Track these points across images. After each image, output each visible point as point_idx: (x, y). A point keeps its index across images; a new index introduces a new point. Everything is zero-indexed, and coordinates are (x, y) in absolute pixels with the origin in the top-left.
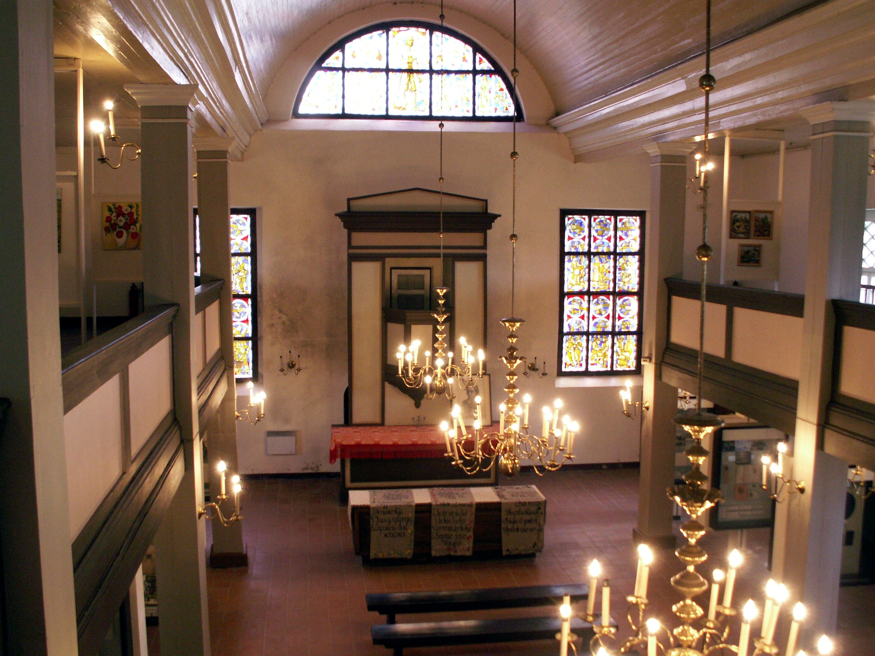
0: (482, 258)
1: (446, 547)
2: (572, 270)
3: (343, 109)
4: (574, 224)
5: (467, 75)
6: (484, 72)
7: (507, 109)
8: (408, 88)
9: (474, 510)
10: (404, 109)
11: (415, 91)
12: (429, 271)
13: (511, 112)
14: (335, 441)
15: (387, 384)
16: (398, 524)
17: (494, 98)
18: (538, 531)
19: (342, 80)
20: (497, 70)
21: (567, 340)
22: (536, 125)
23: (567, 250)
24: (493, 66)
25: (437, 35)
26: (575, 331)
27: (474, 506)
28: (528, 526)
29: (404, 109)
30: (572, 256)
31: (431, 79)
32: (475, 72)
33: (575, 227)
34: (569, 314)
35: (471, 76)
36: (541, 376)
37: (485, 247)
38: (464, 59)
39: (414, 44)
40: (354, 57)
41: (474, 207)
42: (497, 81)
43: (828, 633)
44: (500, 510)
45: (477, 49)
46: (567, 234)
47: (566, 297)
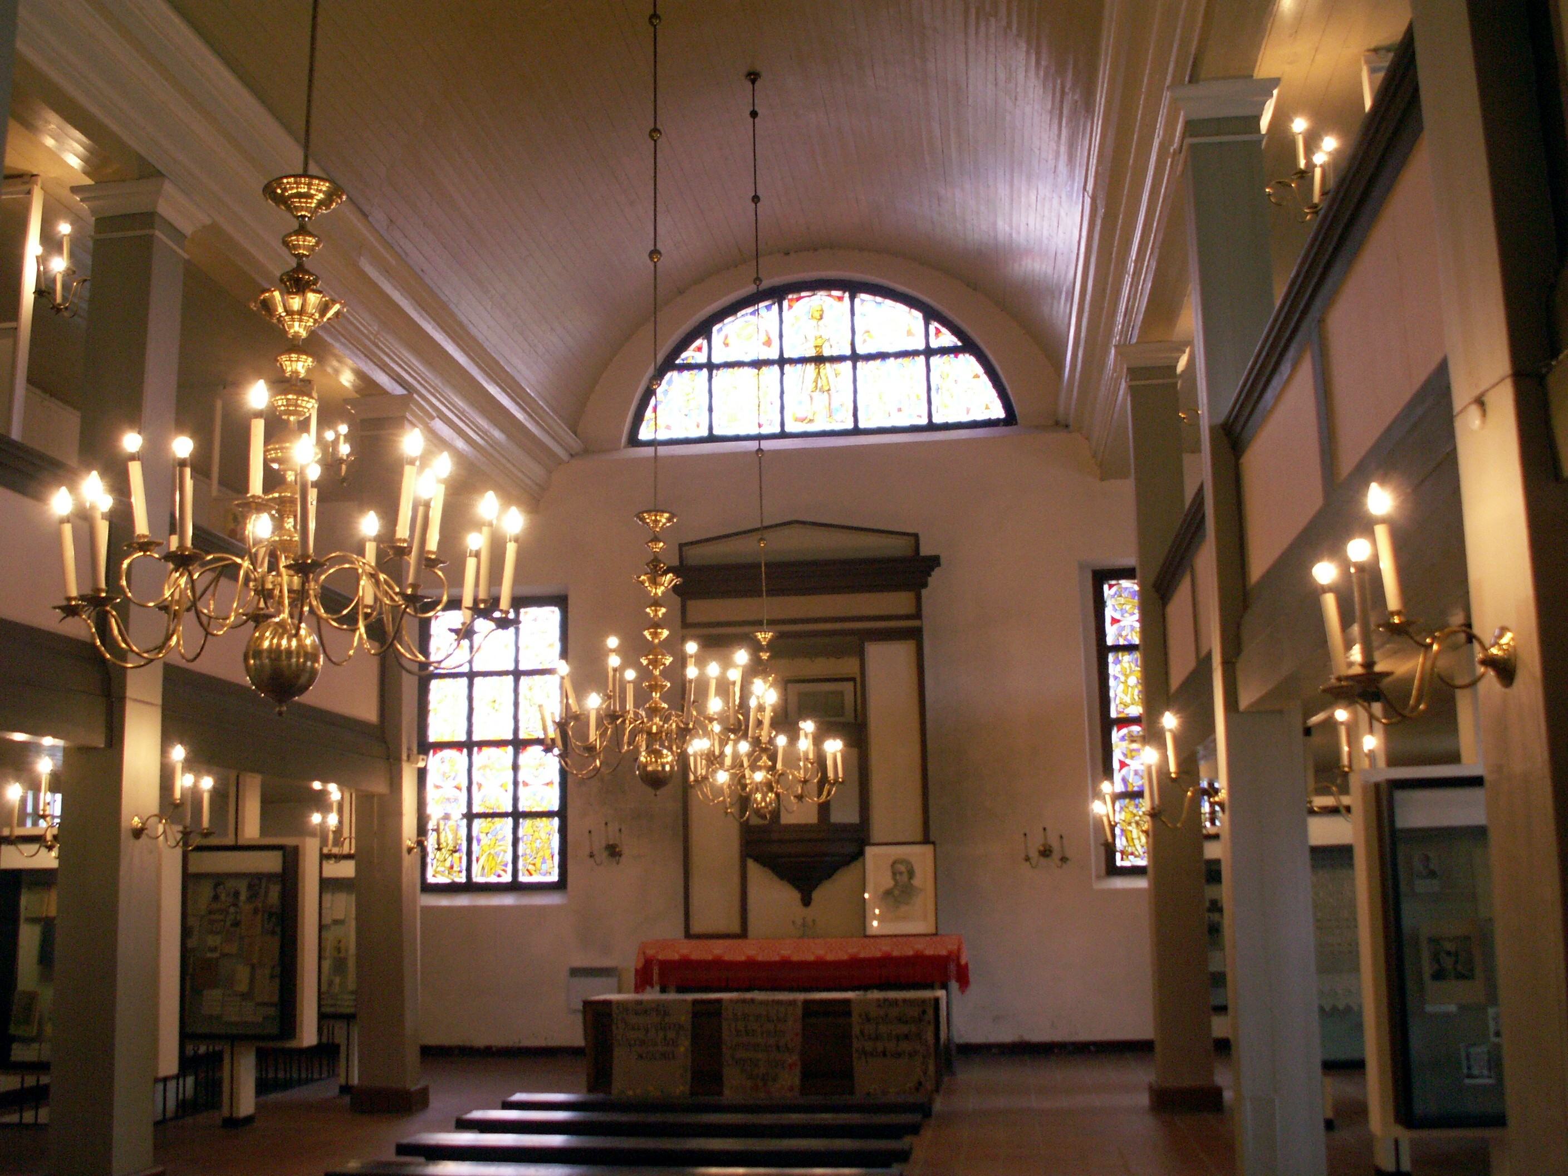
0: (915, 635)
1: (749, 1083)
2: (1122, 679)
3: (711, 428)
4: (1121, 596)
5: (916, 358)
6: (943, 351)
7: (987, 408)
8: (816, 387)
9: (799, 1012)
10: (811, 421)
11: (829, 390)
12: (852, 684)
13: (1001, 414)
14: (644, 953)
15: (751, 863)
16: (661, 1035)
17: (967, 393)
18: (924, 1057)
19: (707, 384)
20: (968, 346)
21: (1121, 808)
22: (1037, 427)
23: (1110, 641)
24: (960, 339)
25: (865, 302)
26: (1136, 789)
27: (800, 1004)
28: (905, 1046)
29: (811, 421)
30: (1120, 654)
31: (855, 368)
32: (929, 352)
33: (1122, 600)
34: (1122, 758)
35: (922, 358)
36: (1059, 863)
37: (918, 615)
38: (909, 333)
39: (824, 316)
40: (727, 345)
41: (896, 547)
42: (968, 363)
43: (755, 677)
44: (849, 1014)
45: (930, 315)
46: (1109, 613)
47: (1115, 729)
